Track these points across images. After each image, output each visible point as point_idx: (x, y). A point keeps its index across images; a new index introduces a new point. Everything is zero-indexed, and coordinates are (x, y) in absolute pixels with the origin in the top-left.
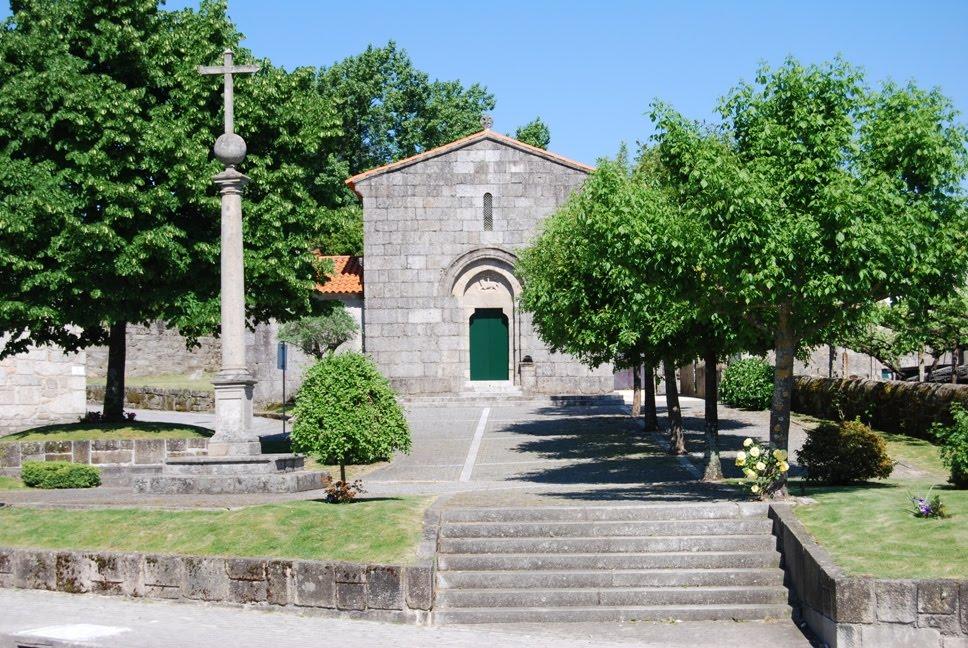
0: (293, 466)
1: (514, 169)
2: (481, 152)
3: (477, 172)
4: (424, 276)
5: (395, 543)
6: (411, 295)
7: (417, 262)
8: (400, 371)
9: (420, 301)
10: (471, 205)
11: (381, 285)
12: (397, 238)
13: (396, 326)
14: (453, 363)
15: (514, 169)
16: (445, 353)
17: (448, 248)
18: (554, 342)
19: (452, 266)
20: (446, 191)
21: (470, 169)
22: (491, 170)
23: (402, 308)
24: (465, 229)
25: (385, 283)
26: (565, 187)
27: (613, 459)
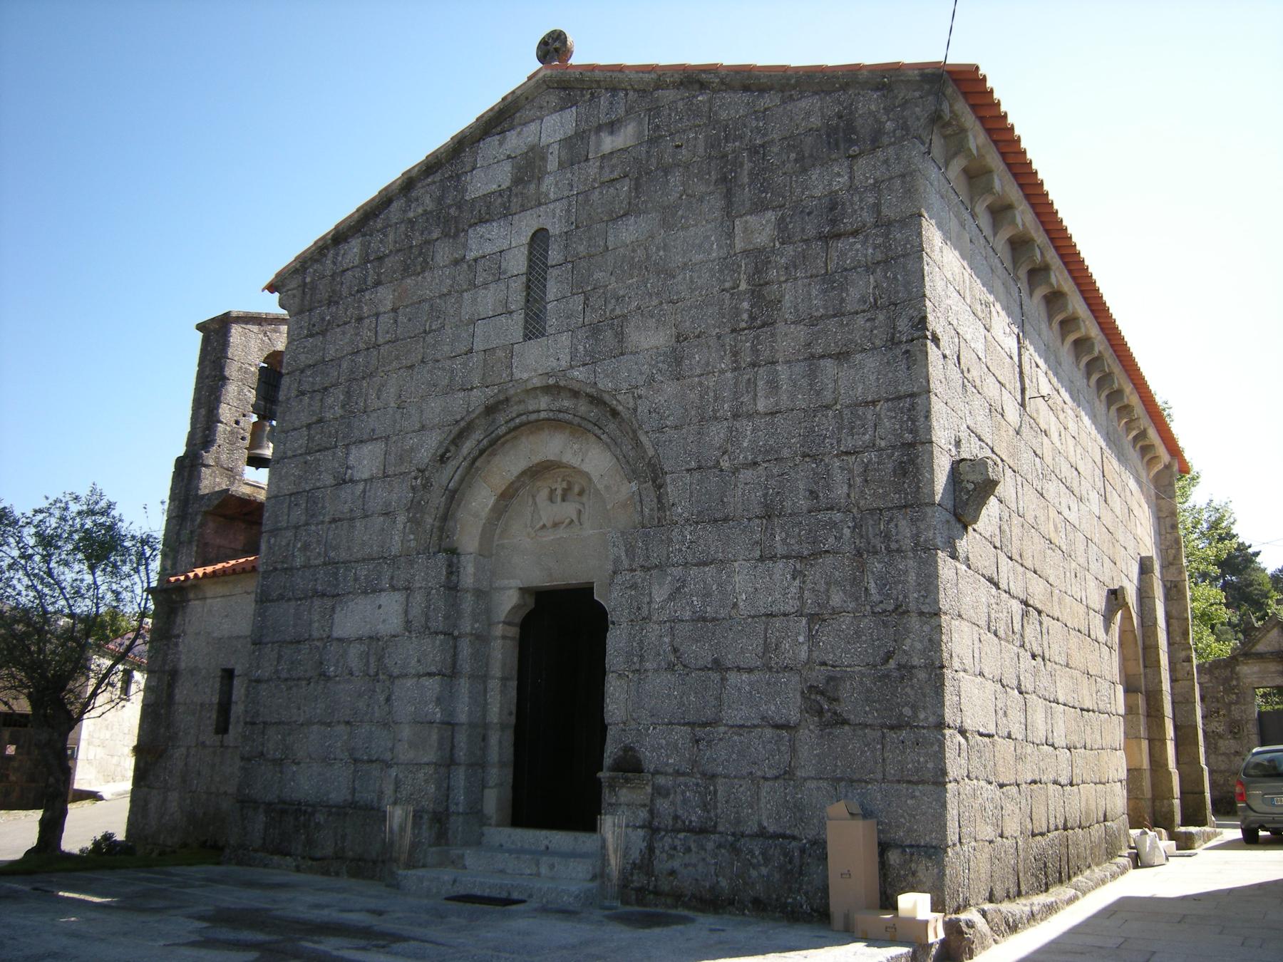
0: (238, 941)
1: (609, 143)
2: (533, 127)
3: (517, 181)
4: (380, 496)
5: (624, 215)
6: (344, 555)
7: (366, 460)
8: (610, 721)
9: (363, 571)
10: (499, 275)
11: (290, 534)
12: (334, 406)
13: (305, 648)
14: (420, 765)
15: (609, 143)
16: (406, 732)
17: (435, 408)
18: (1253, 562)
19: (443, 459)
20: (443, 253)
21: (502, 176)
22: (552, 164)
23: (323, 595)
24: (479, 345)
25: (297, 527)
26: (753, 151)
27: (233, 562)
